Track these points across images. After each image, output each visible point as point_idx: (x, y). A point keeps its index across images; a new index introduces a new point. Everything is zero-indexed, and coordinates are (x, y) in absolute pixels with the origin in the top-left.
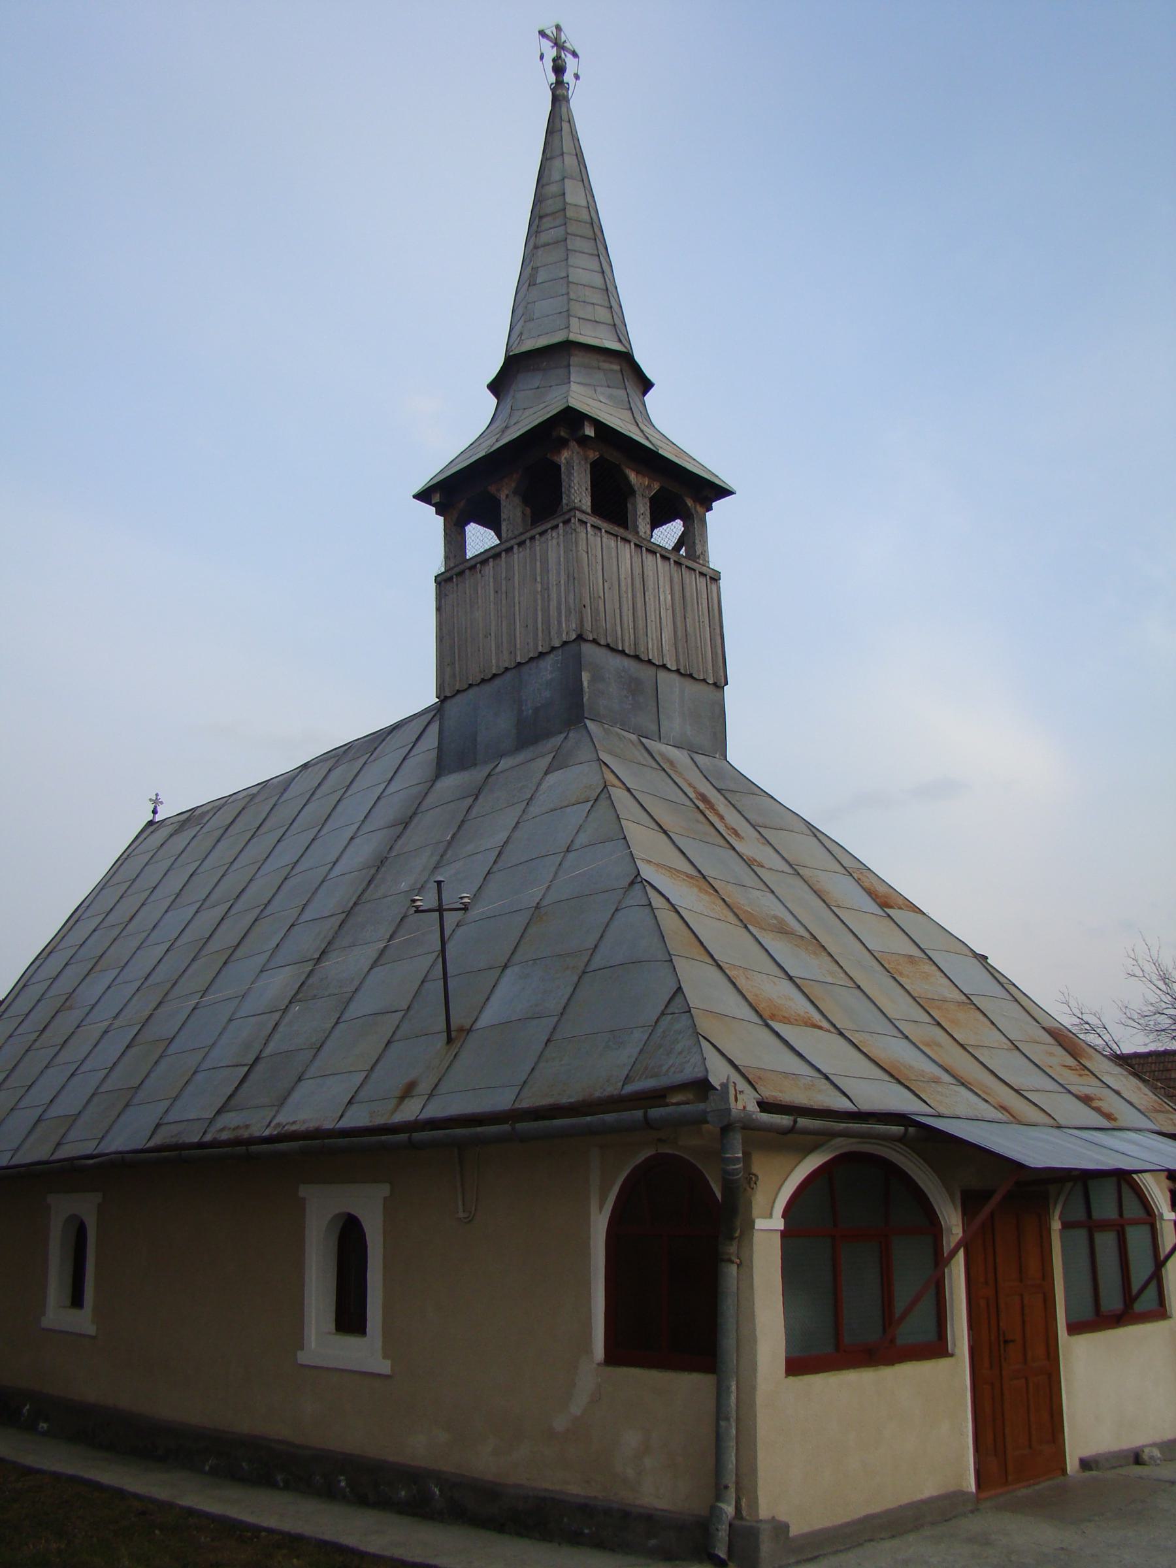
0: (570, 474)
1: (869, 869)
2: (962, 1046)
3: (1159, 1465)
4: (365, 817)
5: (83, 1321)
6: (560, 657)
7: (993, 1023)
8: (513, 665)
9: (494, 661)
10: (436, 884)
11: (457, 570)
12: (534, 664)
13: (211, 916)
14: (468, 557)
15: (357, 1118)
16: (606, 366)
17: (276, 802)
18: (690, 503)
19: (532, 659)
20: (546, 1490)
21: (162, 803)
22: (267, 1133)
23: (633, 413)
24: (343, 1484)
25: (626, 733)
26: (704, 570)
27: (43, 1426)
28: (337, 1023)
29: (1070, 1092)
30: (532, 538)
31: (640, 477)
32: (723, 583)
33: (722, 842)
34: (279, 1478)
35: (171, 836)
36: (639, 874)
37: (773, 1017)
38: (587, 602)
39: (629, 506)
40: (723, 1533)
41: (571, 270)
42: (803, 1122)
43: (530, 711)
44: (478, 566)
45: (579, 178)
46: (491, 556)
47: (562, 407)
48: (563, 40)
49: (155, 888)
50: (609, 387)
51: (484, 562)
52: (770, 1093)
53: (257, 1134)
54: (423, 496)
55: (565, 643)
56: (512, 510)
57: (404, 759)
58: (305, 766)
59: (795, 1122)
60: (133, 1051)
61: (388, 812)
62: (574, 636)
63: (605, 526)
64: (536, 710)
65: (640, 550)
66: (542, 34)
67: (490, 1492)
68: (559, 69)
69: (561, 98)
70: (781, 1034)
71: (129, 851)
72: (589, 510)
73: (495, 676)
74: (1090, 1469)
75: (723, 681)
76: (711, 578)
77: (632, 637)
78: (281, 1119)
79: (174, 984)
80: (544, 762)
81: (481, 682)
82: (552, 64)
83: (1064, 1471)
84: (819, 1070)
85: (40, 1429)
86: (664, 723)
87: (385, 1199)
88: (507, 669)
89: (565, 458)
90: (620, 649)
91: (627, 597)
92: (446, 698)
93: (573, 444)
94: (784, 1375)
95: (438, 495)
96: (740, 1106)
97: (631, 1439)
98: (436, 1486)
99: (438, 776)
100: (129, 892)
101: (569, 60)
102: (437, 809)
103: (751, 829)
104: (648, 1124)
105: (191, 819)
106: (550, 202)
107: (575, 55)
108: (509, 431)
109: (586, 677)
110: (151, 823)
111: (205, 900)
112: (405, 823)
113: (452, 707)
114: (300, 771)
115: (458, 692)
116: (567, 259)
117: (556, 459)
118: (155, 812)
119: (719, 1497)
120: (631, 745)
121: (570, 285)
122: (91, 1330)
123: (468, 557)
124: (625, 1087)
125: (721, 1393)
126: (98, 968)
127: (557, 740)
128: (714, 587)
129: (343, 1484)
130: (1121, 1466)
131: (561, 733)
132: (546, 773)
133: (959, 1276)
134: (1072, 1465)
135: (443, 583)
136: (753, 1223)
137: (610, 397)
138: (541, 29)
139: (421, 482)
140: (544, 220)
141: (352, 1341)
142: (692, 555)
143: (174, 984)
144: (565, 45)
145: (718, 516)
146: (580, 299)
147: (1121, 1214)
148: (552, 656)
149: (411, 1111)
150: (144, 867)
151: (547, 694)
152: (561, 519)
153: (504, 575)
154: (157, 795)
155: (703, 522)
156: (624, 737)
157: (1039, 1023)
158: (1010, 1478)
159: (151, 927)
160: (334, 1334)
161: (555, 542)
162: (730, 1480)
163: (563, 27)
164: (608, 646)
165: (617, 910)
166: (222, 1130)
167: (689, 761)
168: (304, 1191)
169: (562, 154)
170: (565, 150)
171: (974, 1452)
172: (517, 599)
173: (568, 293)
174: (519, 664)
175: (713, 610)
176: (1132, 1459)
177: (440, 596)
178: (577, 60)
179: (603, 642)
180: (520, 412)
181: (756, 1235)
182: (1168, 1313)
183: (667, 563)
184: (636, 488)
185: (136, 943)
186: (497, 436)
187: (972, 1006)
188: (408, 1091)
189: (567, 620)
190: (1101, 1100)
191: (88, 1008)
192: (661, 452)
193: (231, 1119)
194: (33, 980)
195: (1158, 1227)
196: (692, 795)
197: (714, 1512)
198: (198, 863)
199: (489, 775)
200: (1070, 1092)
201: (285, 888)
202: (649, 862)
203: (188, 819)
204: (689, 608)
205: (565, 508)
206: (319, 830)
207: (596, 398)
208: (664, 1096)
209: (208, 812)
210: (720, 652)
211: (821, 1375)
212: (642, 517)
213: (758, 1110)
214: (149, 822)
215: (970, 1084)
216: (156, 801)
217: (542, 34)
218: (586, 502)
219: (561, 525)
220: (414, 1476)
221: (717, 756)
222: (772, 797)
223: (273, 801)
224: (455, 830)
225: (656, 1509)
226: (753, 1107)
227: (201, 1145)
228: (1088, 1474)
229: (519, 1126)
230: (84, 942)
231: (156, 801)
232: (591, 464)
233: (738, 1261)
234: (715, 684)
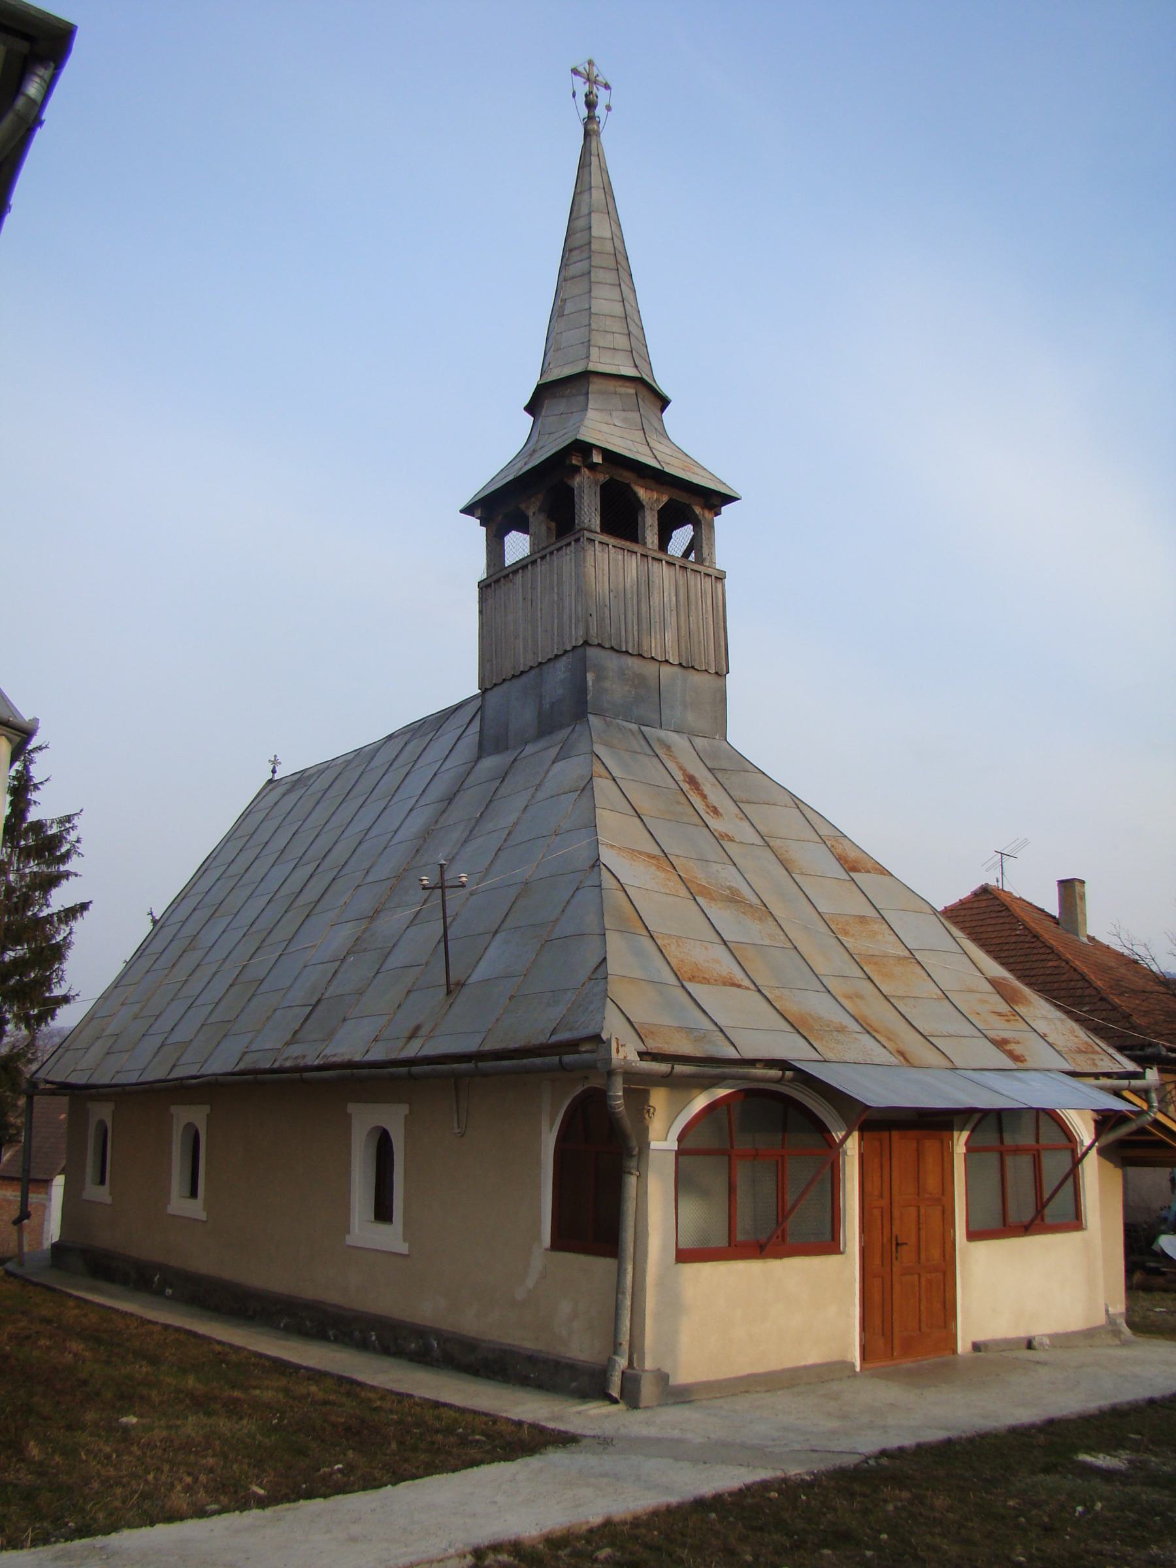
0: (581, 497)
1: (846, 836)
2: (885, 996)
3: (1047, 1350)
4: (423, 791)
5: (195, 1209)
6: (570, 660)
7: (929, 975)
8: (536, 664)
9: (522, 660)
11: (495, 578)
12: (551, 664)
13: (303, 872)
14: (506, 565)
15: (378, 1054)
16: (622, 390)
17: (364, 769)
18: (698, 510)
19: (550, 660)
20: (509, 1345)
21: (280, 763)
22: (316, 1063)
23: (645, 433)
24: (374, 1338)
25: (628, 723)
26: (710, 571)
27: (169, 1291)
28: (377, 973)
29: (986, 1037)
30: (551, 553)
31: (649, 492)
33: (698, 821)
34: (331, 1333)
35: (284, 795)
36: (599, 859)
37: (692, 979)
38: (593, 610)
39: (640, 518)
40: (616, 1379)
41: (593, 302)
42: (680, 1068)
43: (548, 706)
44: (511, 575)
45: (606, 211)
46: (522, 566)
47: (570, 441)
48: (595, 74)
49: (267, 843)
50: (624, 410)
51: (515, 572)
52: (653, 1045)
53: (310, 1063)
54: (468, 510)
55: (574, 647)
56: (538, 521)
57: (458, 739)
58: (390, 737)
60: (233, 990)
61: (440, 788)
62: (581, 642)
63: (612, 541)
64: (553, 705)
65: (646, 560)
66: (575, 72)
67: (470, 1345)
68: (591, 105)
69: (591, 133)
70: (693, 994)
71: (251, 807)
72: (599, 531)
73: (522, 673)
74: (980, 1351)
75: (725, 670)
76: (716, 577)
77: (636, 637)
78: (328, 1051)
79: (270, 933)
80: (554, 752)
81: (512, 678)
82: (584, 99)
83: (954, 1351)
84: (716, 1024)
85: (167, 1294)
86: (666, 712)
87: (406, 1117)
88: (531, 668)
89: (578, 484)
90: (624, 650)
91: (632, 604)
92: (486, 690)
93: (586, 472)
94: (674, 1261)
95: (480, 512)
96: (621, 1056)
97: (565, 1307)
98: (435, 1340)
99: (479, 758)
100: (248, 845)
101: (602, 96)
102: (475, 787)
103: (734, 805)
104: (562, 1067)
105: (302, 779)
106: (578, 235)
107: (607, 87)
108: (536, 455)
109: (590, 677)
110: (270, 781)
111: (301, 858)
112: (450, 799)
113: (492, 697)
114: (385, 742)
115: (495, 685)
116: (590, 292)
117: (570, 482)
118: (274, 771)
119: (615, 1352)
120: (630, 734)
121: (593, 316)
122: (203, 1216)
123: (506, 565)
124: (552, 1037)
125: (620, 1272)
126: (217, 915)
127: (563, 734)
128: (719, 586)
129: (374, 1338)
130: (1011, 1350)
131: (569, 726)
132: (553, 763)
133: (853, 1189)
134: (963, 1346)
135: (484, 589)
136: (648, 1144)
137: (625, 420)
138: (573, 67)
139: (466, 499)
140: (575, 253)
141: (382, 1227)
142: (700, 560)
143: (270, 933)
144: (597, 78)
145: (725, 522)
146: (601, 329)
147: (1037, 1141)
148: (564, 658)
149: (412, 1050)
150: (260, 824)
151: (560, 691)
152: (573, 538)
153: (529, 585)
154: (275, 756)
155: (711, 526)
157: (983, 974)
158: (895, 1354)
159: (260, 880)
160: (372, 1222)
161: (568, 557)
162: (625, 1339)
163: (595, 62)
164: (612, 648)
165: (577, 889)
166: (287, 1059)
167: (688, 744)
168: (352, 1108)
169: (590, 188)
170: (593, 185)
171: (860, 1332)
172: (574, 580)
173: (590, 325)
174: (541, 663)
175: (717, 607)
176: (1024, 1345)
177: (482, 600)
178: (609, 91)
179: (607, 646)
180: (546, 436)
181: (652, 1155)
182: (1084, 1226)
183: (673, 567)
184: (644, 503)
185: (248, 892)
186: (526, 459)
187: (914, 961)
188: (413, 1035)
189: (576, 628)
191: (207, 949)
192: (667, 469)
193: (296, 1050)
194: (167, 924)
196: (679, 776)
197: (611, 1363)
198: (300, 823)
199: (515, 760)
200: (986, 1037)
201: (358, 852)
202: (613, 846)
203: (299, 780)
204: (693, 607)
205: (577, 527)
206: (390, 800)
207: (611, 422)
208: (577, 1045)
209: (314, 774)
210: (723, 644)
211: (709, 1264)
214: (269, 780)
215: (876, 1031)
216: (275, 762)
217: (575, 72)
218: (596, 523)
219: (573, 543)
220: (420, 1332)
221: (717, 737)
222: (764, 773)
223: (361, 769)
224: (483, 809)
225: (579, 1360)
226: (633, 1057)
227: (272, 1071)
229: (480, 1064)
230: (209, 890)
231: (275, 762)
232: (602, 487)
233: (638, 1173)
234: (717, 673)
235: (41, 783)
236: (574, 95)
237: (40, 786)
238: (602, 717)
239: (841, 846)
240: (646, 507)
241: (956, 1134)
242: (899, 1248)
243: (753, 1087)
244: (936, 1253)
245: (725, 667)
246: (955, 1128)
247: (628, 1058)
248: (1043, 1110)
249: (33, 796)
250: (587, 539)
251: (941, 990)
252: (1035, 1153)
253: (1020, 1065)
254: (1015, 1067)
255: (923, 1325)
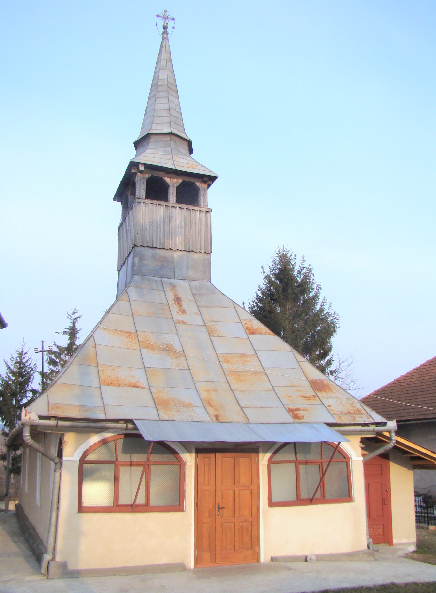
10: (41, 343)
16: (164, 139)
26: (203, 209)
32: (212, 213)
42: (61, 423)
50: (164, 147)
59: (57, 423)
72: (145, 198)
76: (206, 211)
90: (155, 246)
91: (160, 227)
96: (27, 417)
101: (170, 24)
107: (173, 19)
134: (264, 557)
146: (158, 116)
156: (152, 280)
176: (304, 559)
178: (174, 21)
183: (183, 209)
184: (169, 184)
190: (306, 410)
195: (351, 463)
212: (172, 194)
213: (38, 419)
228: (272, 563)
235: (79, 330)
236: (157, 25)
237: (79, 332)
238: (141, 276)
239: (250, 323)
240: (170, 185)
241: (261, 455)
242: (221, 510)
243: (129, 433)
244: (246, 513)
245: (210, 250)
246: (260, 450)
247: (32, 419)
248: (325, 442)
249: (77, 335)
250: (137, 202)
251: (272, 386)
252: (321, 464)
253: (297, 421)
254: (293, 422)
255: (236, 547)
